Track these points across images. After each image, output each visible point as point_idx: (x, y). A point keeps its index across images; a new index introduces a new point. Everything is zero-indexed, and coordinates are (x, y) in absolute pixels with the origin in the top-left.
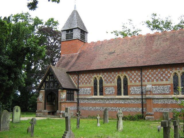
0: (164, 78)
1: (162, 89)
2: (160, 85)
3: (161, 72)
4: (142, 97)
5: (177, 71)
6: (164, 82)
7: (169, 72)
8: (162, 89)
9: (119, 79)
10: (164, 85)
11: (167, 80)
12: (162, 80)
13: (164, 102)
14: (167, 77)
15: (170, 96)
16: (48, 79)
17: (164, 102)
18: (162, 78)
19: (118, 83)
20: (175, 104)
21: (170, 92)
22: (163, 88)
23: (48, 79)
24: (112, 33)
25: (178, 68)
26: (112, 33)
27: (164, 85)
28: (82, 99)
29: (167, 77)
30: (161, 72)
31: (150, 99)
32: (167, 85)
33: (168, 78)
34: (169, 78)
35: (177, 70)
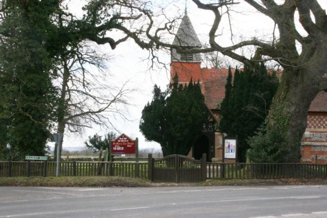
0: (322, 125)
2: (318, 132)
12: (319, 127)
14: (319, 125)
18: (315, 125)
27: (322, 132)
29: (324, 125)
32: (324, 132)
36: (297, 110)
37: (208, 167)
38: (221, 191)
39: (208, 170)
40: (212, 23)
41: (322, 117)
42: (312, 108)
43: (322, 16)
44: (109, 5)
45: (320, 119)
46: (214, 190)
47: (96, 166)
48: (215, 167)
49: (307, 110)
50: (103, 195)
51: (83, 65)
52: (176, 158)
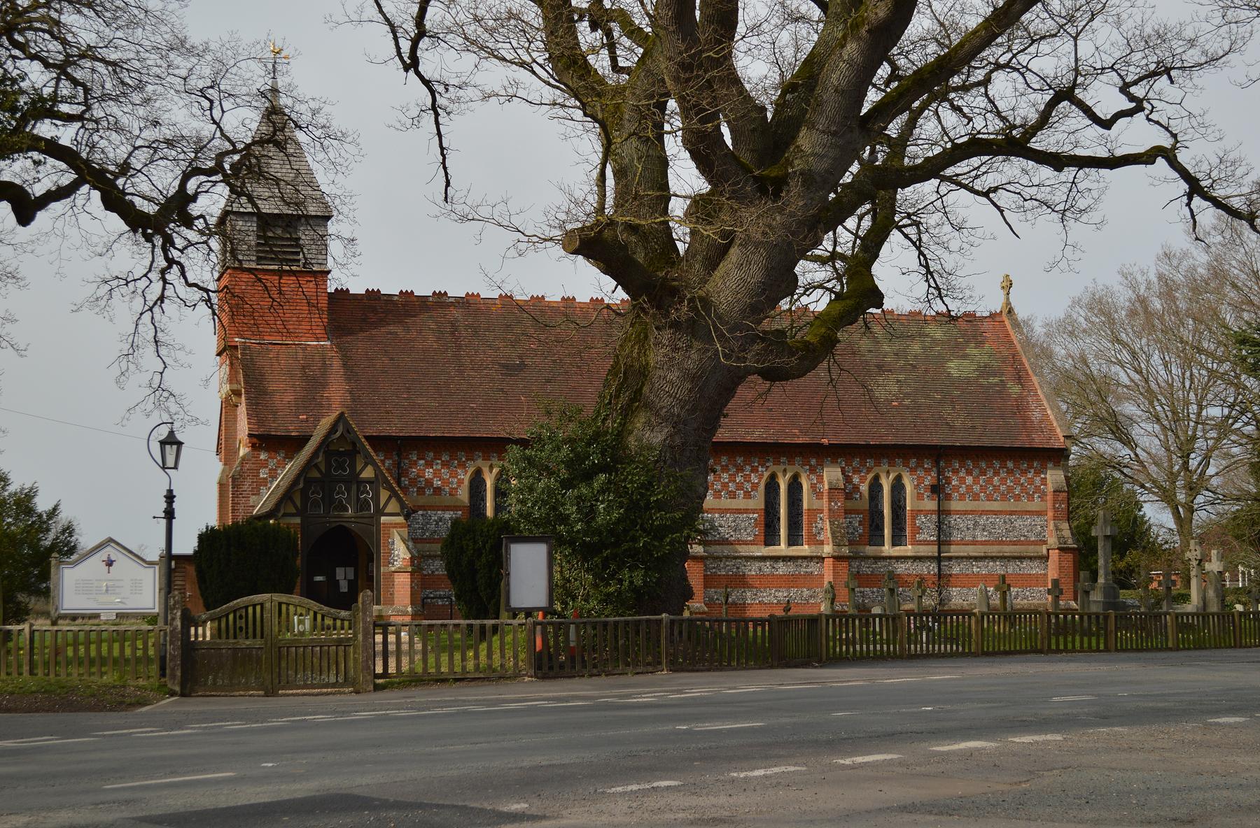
0: (740, 487)
1: (733, 524)
2: (727, 511)
3: (730, 467)
4: (939, 552)
5: (778, 469)
6: (740, 503)
7: (754, 470)
8: (733, 524)
9: (772, 487)
10: (739, 513)
11: (748, 495)
12: (732, 495)
13: (738, 568)
14: (748, 486)
15: (753, 548)
16: (298, 503)
17: (738, 568)
18: (732, 487)
19: (766, 502)
20: (768, 575)
21: (755, 535)
22: (734, 521)
23: (298, 503)
24: (1008, 285)
25: (783, 459)
26: (1008, 285)
27: (739, 511)
28: (957, 558)
29: (748, 486)
30: (730, 467)
31: (719, 558)
32: (746, 511)
33: (752, 491)
34: (757, 491)
35: (778, 463)
36: (678, 441)
37: (379, 638)
38: (732, 732)
39: (379, 648)
40: (1097, 111)
41: (740, 460)
42: (723, 434)
43: (754, 130)
44: (997, 45)
45: (735, 465)
46: (201, 708)
47: (43, 639)
48: (960, 649)
49: (710, 438)
50: (797, 768)
51: (200, 303)
52: (268, 605)
